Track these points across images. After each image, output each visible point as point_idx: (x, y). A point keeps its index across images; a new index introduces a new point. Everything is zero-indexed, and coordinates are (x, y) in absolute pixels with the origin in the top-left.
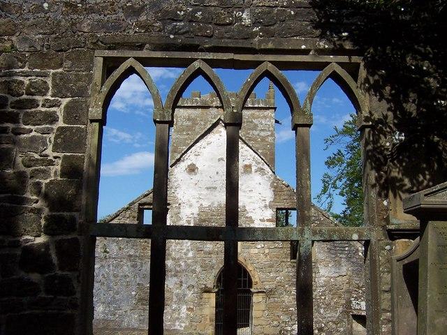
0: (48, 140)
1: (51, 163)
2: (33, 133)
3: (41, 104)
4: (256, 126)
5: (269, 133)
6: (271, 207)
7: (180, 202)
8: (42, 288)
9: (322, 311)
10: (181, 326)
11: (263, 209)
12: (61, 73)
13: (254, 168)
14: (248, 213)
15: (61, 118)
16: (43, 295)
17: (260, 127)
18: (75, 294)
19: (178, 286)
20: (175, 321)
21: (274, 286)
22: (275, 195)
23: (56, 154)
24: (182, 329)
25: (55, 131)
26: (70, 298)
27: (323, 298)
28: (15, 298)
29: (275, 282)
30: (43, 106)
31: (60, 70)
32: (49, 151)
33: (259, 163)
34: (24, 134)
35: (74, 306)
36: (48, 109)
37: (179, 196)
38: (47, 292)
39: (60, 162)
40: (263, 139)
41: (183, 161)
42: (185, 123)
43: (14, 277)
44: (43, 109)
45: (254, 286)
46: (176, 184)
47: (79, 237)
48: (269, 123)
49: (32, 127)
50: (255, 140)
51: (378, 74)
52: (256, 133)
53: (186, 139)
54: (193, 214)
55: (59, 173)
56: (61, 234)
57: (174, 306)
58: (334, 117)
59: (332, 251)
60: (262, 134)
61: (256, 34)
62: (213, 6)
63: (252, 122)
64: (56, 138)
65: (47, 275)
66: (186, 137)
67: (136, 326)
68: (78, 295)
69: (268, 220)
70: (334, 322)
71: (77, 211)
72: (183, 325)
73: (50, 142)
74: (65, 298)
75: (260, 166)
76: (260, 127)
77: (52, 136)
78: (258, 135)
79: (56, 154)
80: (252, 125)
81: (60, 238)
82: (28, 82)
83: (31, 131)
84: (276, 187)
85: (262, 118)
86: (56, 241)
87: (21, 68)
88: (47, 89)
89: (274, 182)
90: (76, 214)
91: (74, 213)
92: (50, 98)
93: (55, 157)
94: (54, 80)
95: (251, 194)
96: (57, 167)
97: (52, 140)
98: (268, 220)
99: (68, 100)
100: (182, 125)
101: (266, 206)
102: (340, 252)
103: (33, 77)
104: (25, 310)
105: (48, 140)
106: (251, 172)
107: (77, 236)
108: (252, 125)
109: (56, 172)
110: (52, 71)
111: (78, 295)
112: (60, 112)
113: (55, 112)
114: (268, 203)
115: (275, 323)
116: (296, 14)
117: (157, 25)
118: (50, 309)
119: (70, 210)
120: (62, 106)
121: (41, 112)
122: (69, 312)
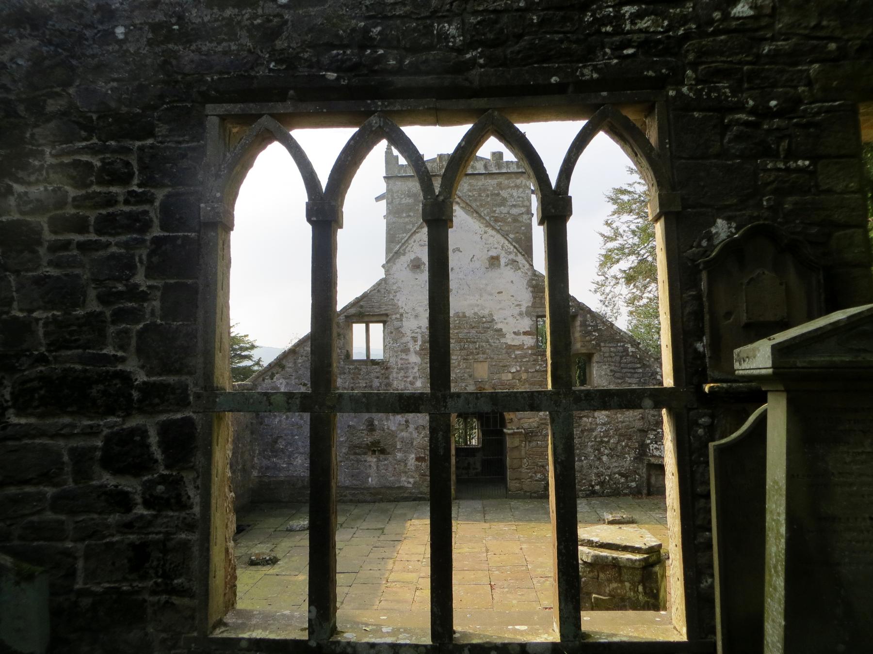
0: (137, 259)
1: (144, 297)
2: (114, 249)
3: (121, 199)
4: (504, 200)
5: (523, 210)
6: (528, 314)
7: (401, 311)
8: (139, 500)
9: (605, 458)
10: (409, 483)
11: (518, 317)
12: (152, 147)
13: (503, 261)
14: (496, 323)
15: (156, 222)
16: (140, 510)
17: (511, 202)
18: (191, 507)
19: (404, 427)
20: (400, 474)
21: (535, 425)
22: (534, 298)
23: (149, 283)
24: (410, 486)
25: (148, 243)
26: (183, 514)
27: (606, 439)
28: (95, 516)
29: (537, 419)
30: (127, 202)
31: (150, 141)
32: (140, 279)
33: (510, 253)
34: (97, 250)
35: (190, 527)
36: (134, 208)
37: (400, 304)
38: (147, 504)
39: (159, 294)
40: (515, 220)
41: (404, 254)
42: (404, 201)
43: (94, 483)
44: (127, 209)
45: (509, 426)
46: (395, 287)
47: (194, 416)
48: (522, 195)
49: (111, 239)
50: (503, 220)
51: (703, 247)
52: (504, 210)
53: (406, 223)
54: (420, 328)
55: (158, 312)
56: (168, 412)
57: (399, 455)
58: (438, 622)
59: (617, 375)
60: (514, 211)
61: (473, 62)
62: (399, 16)
63: (498, 194)
64: (149, 256)
65: (146, 478)
66: (407, 220)
67: (347, 483)
68: (197, 509)
69: (525, 333)
70: (622, 475)
71: (190, 373)
72: (411, 480)
73: (141, 261)
74: (176, 514)
75: (512, 257)
76: (511, 202)
77: (144, 252)
78: (508, 213)
79: (149, 283)
80: (499, 199)
81: (164, 417)
82: (99, 164)
83: (108, 245)
84: (534, 287)
85: (513, 188)
86: (157, 423)
87: (85, 139)
88: (131, 175)
89: (533, 280)
90: (189, 380)
91: (183, 378)
92: (135, 188)
93: (149, 287)
94: (140, 160)
95: (499, 297)
96: (154, 303)
97: (144, 257)
98: (525, 333)
99: (166, 191)
100: (400, 204)
101: (521, 314)
102: (629, 375)
103: (108, 155)
104: (113, 535)
105: (137, 259)
106: (499, 266)
107: (191, 414)
108: (499, 199)
109: (153, 313)
110: (138, 143)
111: (197, 509)
112: (154, 212)
113: (146, 212)
114: (524, 309)
115: (539, 476)
116: (542, 22)
117: (306, 56)
118: (153, 533)
119: (178, 372)
120: (157, 204)
121: (123, 213)
122: (183, 536)
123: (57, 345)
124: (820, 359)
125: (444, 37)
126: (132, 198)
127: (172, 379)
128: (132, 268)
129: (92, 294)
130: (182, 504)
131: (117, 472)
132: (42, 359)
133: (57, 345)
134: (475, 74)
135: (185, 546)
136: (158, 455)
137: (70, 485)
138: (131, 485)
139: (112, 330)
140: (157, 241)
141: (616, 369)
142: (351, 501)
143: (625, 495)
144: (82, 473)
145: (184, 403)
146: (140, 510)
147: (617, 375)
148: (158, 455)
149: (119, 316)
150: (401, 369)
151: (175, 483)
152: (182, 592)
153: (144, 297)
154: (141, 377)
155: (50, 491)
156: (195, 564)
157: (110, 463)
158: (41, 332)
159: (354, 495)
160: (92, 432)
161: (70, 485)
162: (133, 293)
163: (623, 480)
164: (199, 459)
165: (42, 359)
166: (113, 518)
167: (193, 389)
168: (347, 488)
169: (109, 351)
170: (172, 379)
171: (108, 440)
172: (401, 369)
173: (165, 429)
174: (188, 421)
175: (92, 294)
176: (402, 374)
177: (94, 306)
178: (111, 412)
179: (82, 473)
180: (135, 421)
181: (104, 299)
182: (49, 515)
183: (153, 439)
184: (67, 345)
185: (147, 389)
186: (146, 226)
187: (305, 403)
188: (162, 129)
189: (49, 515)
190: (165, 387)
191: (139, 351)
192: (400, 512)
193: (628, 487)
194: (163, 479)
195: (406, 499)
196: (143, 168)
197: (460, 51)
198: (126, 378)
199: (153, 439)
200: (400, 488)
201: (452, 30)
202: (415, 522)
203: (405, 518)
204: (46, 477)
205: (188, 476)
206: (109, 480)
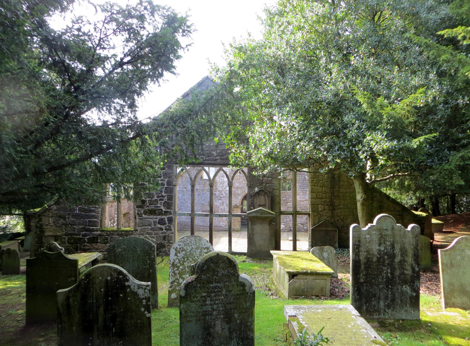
1: (164, 197)
16: (164, 231)
32: (163, 194)
35: (172, 233)
38: (165, 230)
59: (302, 187)
70: (302, 224)
77: (164, 189)
112: (165, 183)
123: (150, 204)
124: (252, 215)
125: (213, 154)
126: (162, 180)
127: (169, 210)
128: (162, 192)
129: (156, 196)
130: (171, 230)
131: (161, 225)
132: (148, 206)
133: (150, 204)
134: (218, 161)
135: (171, 236)
136: (167, 222)
137: (153, 226)
138: (163, 227)
139: (159, 202)
140: (166, 187)
141: (302, 185)
142: (202, 231)
143: (302, 231)
144: (155, 225)
145: (171, 214)
146: (164, 231)
147: (302, 187)
148: (167, 222)
149: (160, 200)
150: (221, 183)
151: (170, 227)
152: (171, 243)
153: (164, 197)
154: (164, 210)
155: (150, 227)
156: (173, 239)
157: (159, 223)
158: (148, 202)
159: (203, 228)
160: (156, 218)
161: (153, 226)
162: (162, 196)
163: (302, 226)
164: (173, 223)
165: (148, 206)
166: (160, 232)
167: (172, 212)
168: (201, 226)
169: (159, 205)
170: (169, 210)
171: (159, 220)
172: (221, 183)
173: (168, 218)
174: (172, 217)
175: (156, 196)
176: (221, 185)
177: (156, 198)
178: (159, 215)
179: (155, 225)
180: (163, 217)
181: (158, 197)
182: (150, 231)
183: (166, 220)
184: (152, 204)
185: (165, 212)
186: (164, 185)
187: (190, 215)
188: (166, 169)
189: (150, 231)
190: (168, 212)
191: (164, 206)
192: (219, 235)
193: (304, 229)
194: (168, 226)
195: (222, 231)
196: (163, 175)
197: (216, 157)
198: (161, 210)
199: (166, 220)
200: (220, 226)
201: (215, 153)
202: (224, 238)
203: (221, 237)
204: (149, 225)
205: (172, 226)
206: (159, 226)
